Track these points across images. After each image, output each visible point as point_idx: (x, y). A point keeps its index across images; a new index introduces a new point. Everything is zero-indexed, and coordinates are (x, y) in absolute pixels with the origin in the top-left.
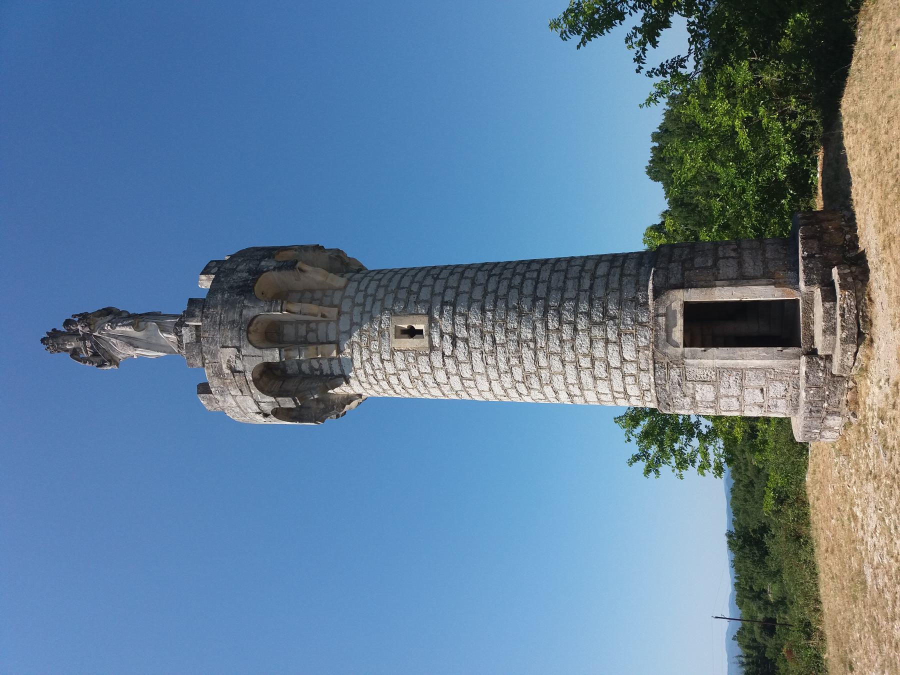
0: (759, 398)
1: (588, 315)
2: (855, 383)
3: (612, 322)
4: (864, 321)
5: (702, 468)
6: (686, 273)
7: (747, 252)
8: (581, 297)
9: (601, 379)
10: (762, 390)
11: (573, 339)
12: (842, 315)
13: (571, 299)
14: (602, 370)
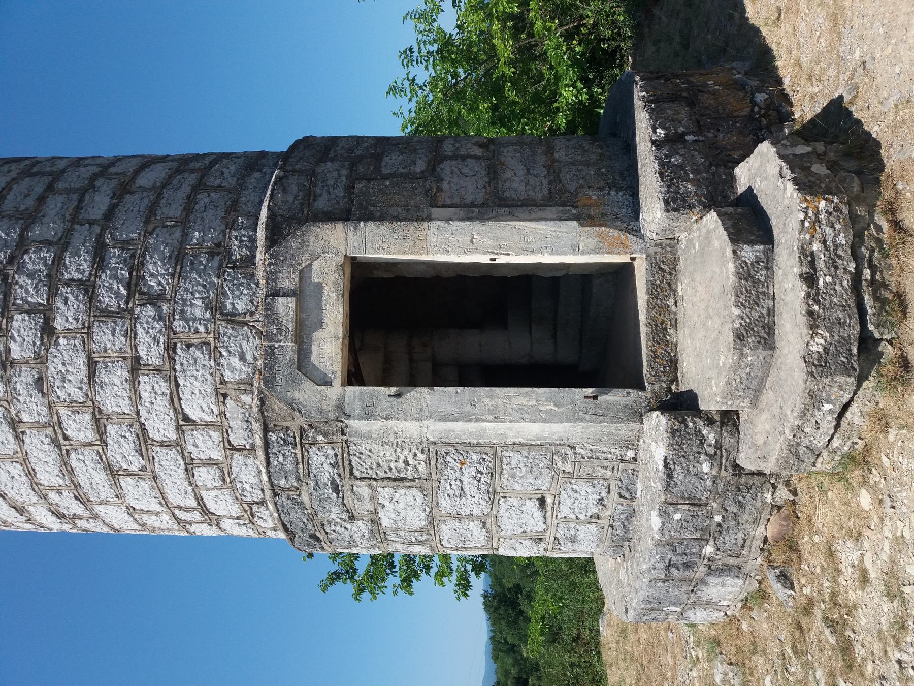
0: (534, 520)
1: (88, 288)
2: (795, 493)
3: (150, 311)
4: (876, 298)
5: (440, 575)
6: (360, 186)
7: (511, 149)
8: (76, 240)
9: (128, 473)
10: (542, 501)
11: (41, 359)
12: (810, 279)
13: (48, 243)
14: (128, 448)
